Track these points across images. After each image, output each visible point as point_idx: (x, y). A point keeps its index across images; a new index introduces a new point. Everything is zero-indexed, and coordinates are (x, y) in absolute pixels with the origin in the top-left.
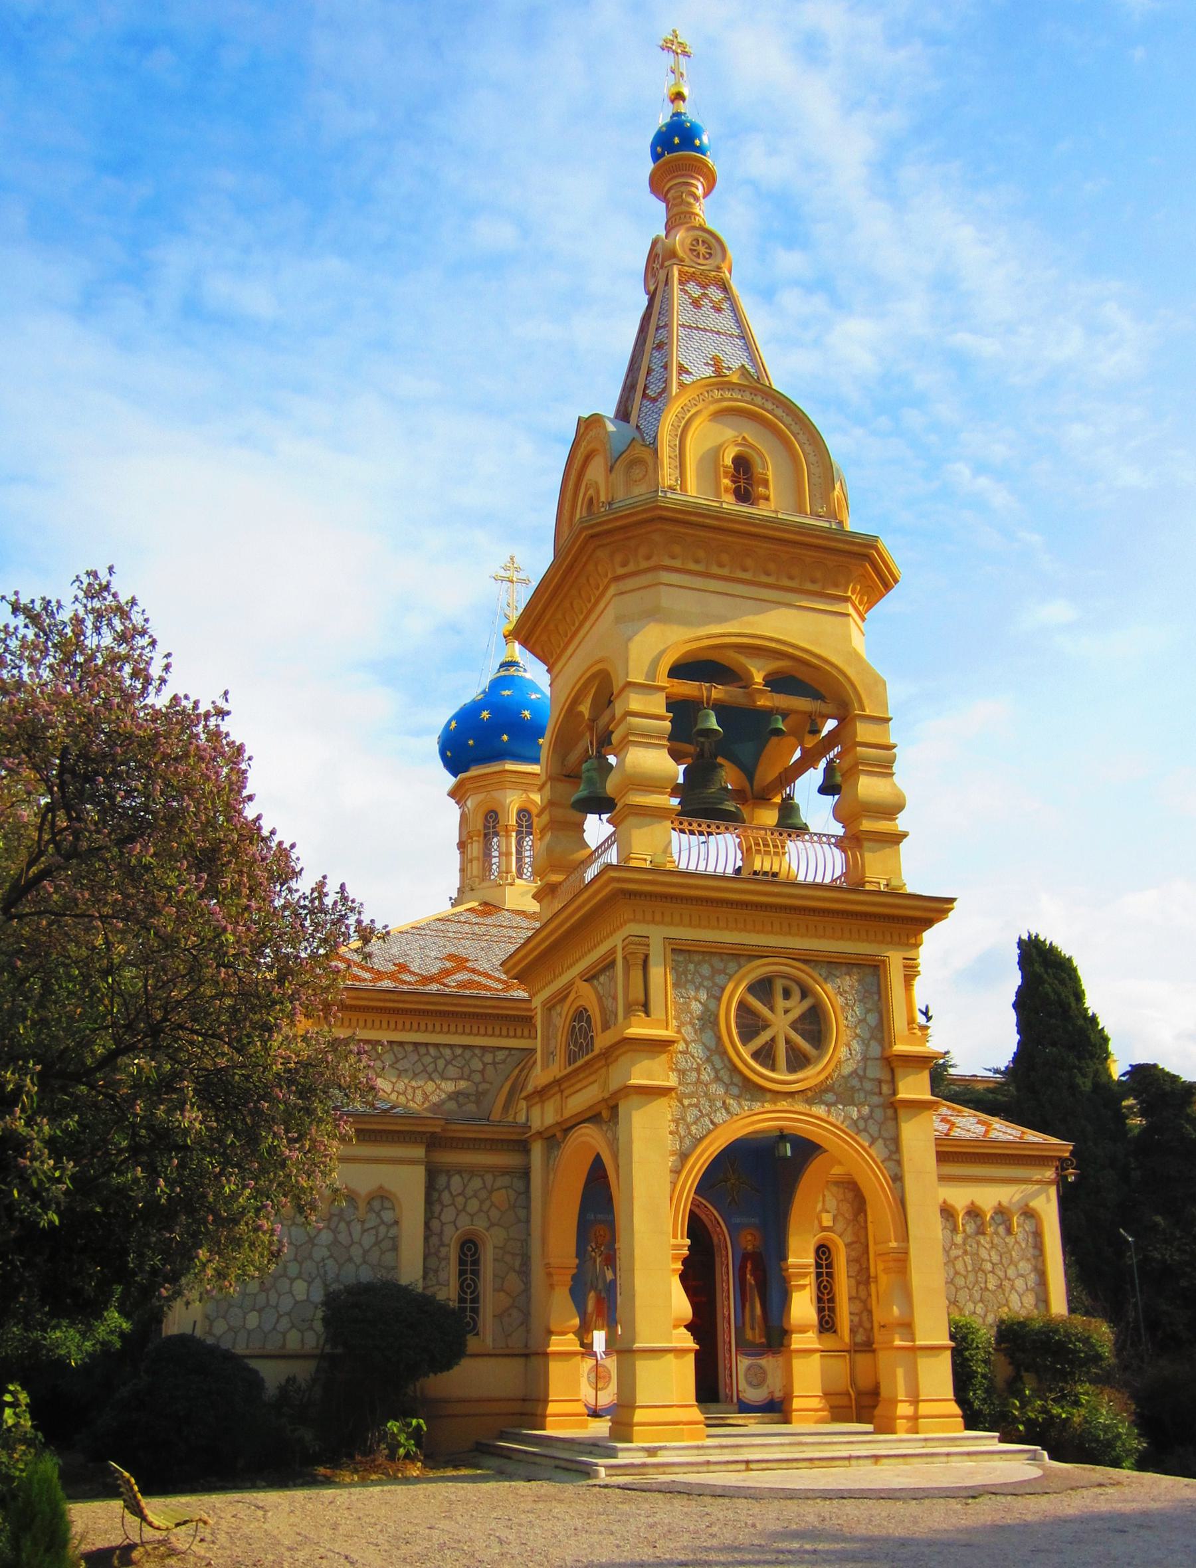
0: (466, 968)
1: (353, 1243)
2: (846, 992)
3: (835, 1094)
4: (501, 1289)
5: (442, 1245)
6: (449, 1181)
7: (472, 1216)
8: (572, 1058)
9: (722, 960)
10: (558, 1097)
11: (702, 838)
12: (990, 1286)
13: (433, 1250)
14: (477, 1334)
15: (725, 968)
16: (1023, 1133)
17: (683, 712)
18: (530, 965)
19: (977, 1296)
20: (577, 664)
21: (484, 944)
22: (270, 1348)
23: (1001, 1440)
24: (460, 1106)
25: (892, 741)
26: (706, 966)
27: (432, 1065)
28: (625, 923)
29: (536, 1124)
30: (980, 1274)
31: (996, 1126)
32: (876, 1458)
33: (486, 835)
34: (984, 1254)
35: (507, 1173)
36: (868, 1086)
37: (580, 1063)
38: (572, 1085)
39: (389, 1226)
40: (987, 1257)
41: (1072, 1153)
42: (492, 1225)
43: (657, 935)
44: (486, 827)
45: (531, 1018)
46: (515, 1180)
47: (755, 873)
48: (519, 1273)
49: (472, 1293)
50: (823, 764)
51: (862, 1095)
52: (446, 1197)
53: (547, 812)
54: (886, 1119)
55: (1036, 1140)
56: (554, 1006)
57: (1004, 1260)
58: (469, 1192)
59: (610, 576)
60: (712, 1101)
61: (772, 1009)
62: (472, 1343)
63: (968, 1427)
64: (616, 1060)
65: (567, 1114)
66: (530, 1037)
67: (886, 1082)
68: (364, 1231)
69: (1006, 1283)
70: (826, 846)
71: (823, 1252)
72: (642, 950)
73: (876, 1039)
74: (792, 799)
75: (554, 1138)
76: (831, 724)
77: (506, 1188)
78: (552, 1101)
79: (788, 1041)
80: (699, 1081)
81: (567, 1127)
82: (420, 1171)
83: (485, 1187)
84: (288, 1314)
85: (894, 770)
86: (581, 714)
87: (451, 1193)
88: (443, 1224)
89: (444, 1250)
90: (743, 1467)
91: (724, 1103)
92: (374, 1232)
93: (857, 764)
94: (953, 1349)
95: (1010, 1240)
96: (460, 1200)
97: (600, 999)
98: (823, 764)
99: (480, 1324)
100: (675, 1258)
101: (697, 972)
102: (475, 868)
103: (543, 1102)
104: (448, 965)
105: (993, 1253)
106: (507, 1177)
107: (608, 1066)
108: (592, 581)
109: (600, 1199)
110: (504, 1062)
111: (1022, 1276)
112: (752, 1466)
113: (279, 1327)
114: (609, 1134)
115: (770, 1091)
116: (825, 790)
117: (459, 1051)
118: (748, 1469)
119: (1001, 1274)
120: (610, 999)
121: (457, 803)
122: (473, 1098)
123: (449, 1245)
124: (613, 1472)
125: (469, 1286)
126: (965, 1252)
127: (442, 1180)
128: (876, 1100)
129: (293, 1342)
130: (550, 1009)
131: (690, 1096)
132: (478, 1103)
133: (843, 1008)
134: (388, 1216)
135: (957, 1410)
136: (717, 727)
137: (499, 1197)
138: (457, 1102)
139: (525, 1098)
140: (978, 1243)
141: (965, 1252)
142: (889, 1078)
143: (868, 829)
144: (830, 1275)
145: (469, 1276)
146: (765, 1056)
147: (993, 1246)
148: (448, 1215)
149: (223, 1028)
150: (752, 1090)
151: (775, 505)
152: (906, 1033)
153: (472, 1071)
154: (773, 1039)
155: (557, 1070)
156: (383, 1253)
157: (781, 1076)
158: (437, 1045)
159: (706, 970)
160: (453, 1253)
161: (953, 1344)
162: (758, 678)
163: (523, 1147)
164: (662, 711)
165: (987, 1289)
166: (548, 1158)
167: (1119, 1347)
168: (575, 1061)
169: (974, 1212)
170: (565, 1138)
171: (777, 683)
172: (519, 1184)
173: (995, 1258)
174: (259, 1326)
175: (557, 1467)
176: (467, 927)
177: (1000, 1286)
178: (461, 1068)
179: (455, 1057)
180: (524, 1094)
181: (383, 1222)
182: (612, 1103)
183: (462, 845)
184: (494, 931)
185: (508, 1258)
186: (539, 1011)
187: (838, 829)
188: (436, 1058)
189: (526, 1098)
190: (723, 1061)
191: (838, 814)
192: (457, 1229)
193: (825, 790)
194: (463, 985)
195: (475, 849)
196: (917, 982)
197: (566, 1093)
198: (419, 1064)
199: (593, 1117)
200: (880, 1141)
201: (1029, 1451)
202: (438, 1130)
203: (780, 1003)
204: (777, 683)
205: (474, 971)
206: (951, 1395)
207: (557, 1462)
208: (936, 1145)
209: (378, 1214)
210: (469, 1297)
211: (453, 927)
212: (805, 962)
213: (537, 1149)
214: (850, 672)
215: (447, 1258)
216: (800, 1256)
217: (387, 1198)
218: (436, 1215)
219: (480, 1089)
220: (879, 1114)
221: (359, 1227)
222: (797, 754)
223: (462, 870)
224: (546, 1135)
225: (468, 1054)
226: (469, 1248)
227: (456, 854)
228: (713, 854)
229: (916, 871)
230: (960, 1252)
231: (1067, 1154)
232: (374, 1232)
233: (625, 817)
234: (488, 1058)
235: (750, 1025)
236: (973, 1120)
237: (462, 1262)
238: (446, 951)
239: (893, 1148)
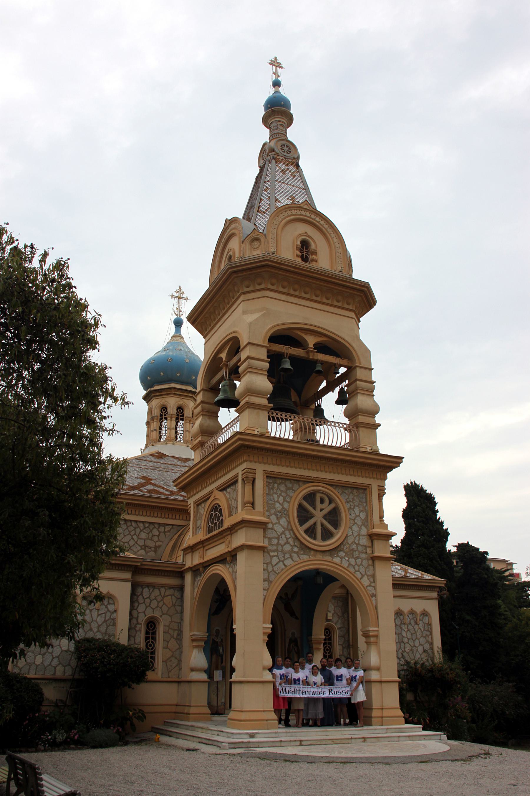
0: (151, 484)
1: (93, 621)
2: (350, 501)
3: (344, 552)
4: (167, 648)
5: (138, 623)
6: (142, 592)
7: (153, 609)
8: (210, 530)
9: (291, 483)
10: (202, 549)
11: (278, 423)
12: (407, 650)
13: (133, 626)
14: (154, 670)
15: (292, 487)
16: (422, 574)
17: (274, 359)
18: (191, 483)
20: (222, 332)
21: (159, 472)
22: (48, 675)
23: (424, 729)
24: (147, 553)
25: (373, 380)
26: (283, 485)
27: (134, 531)
28: (244, 462)
29: (189, 564)
30: (402, 644)
31: (409, 571)
32: (364, 739)
33: (161, 419)
34: (404, 634)
35: (172, 588)
36: (360, 548)
37: (215, 532)
38: (210, 544)
39: (112, 613)
40: (405, 636)
41: (446, 584)
42: (164, 614)
43: (260, 469)
44: (161, 415)
45: (187, 510)
46: (176, 591)
47: (307, 440)
48: (176, 639)
49: (152, 649)
50: (337, 390)
51: (357, 553)
52: (141, 600)
53: (200, 406)
54: (369, 565)
55: (428, 578)
56: (200, 504)
58: (152, 597)
59: (240, 292)
60: (285, 554)
61: (314, 508)
62: (150, 675)
63: (407, 722)
64: (237, 531)
65: (206, 559)
66: (186, 520)
67: (369, 547)
68: (99, 615)
69: (414, 648)
70: (342, 430)
71: (328, 631)
72: (252, 476)
73: (364, 525)
74: (321, 406)
75: (196, 571)
76: (342, 370)
77: (171, 595)
78: (198, 551)
79: (322, 525)
81: (206, 565)
82: (129, 585)
83: (161, 595)
84: (58, 657)
85: (374, 393)
86: (221, 358)
87: (143, 597)
88: (138, 613)
89: (138, 626)
91: (290, 555)
92: (103, 615)
93: (357, 390)
94: (399, 682)
95: (416, 627)
96: (148, 601)
97: (227, 500)
98: (337, 390)
99: (155, 666)
100: (264, 633)
101: (278, 488)
102: (155, 435)
103: (193, 552)
104: (143, 481)
106: (172, 590)
107: (231, 534)
108: (231, 294)
109: (220, 601)
110: (169, 531)
111: (421, 645)
113: (53, 664)
114: (231, 570)
115: (313, 550)
116: (338, 402)
117: (147, 525)
119: (412, 644)
120: (233, 501)
121: (147, 403)
122: (153, 549)
123: (141, 624)
124: (232, 746)
125: (150, 645)
127: (139, 590)
128: (363, 556)
129: (59, 673)
130: (198, 505)
131: (274, 551)
132: (155, 551)
133: (348, 509)
134: (111, 608)
135: (401, 713)
136: (290, 367)
137: (168, 600)
138: (145, 550)
139: (183, 550)
140: (401, 628)
142: (370, 545)
143: (362, 421)
144: (330, 644)
145: (151, 640)
147: (408, 630)
148: (141, 608)
149: (97, 503)
150: (305, 548)
151: (323, 262)
152: (379, 522)
153: (153, 536)
154: (315, 524)
155: (201, 536)
156: (108, 626)
157: (318, 543)
158: (136, 521)
159: (283, 487)
160: (143, 628)
161: (399, 680)
162: (311, 345)
163: (180, 574)
164: (265, 358)
165: (405, 651)
166: (194, 581)
168: (212, 532)
169: (412, 612)
170: (204, 571)
171: (320, 348)
172: (177, 594)
173: (409, 636)
174: (42, 663)
175: (199, 742)
176: (151, 464)
177: (411, 650)
178: (148, 534)
179: (145, 528)
180: (182, 548)
181: (109, 611)
182: (233, 553)
183: (148, 423)
184: (163, 466)
185: (171, 632)
186: (192, 505)
187: (346, 421)
188: (135, 528)
189: (184, 550)
190: (290, 534)
191: (347, 414)
192: (146, 616)
193: (338, 402)
194: (150, 491)
195: (155, 425)
196: (385, 498)
197: (206, 548)
198: (127, 530)
199: (221, 560)
200: (366, 576)
201: (437, 735)
202: (139, 564)
203: (319, 506)
204: (320, 348)
205: (155, 485)
206: (398, 706)
207: (200, 740)
208: (393, 580)
209: (106, 607)
210: (150, 651)
211: (144, 463)
212: (331, 485)
213: (188, 577)
214: (354, 345)
215: (140, 630)
216: (318, 633)
217: (111, 598)
218: (135, 608)
219: (157, 545)
220: (365, 563)
221: (96, 613)
222: (324, 384)
223: (147, 436)
224: (194, 569)
225: (151, 527)
226: (151, 625)
227: (145, 427)
228: (283, 430)
229: (386, 444)
231: (443, 585)
232: (103, 615)
233: (246, 408)
234: (162, 529)
235: (304, 515)
236: (399, 568)
237: (147, 633)
238: (142, 475)
239: (372, 580)
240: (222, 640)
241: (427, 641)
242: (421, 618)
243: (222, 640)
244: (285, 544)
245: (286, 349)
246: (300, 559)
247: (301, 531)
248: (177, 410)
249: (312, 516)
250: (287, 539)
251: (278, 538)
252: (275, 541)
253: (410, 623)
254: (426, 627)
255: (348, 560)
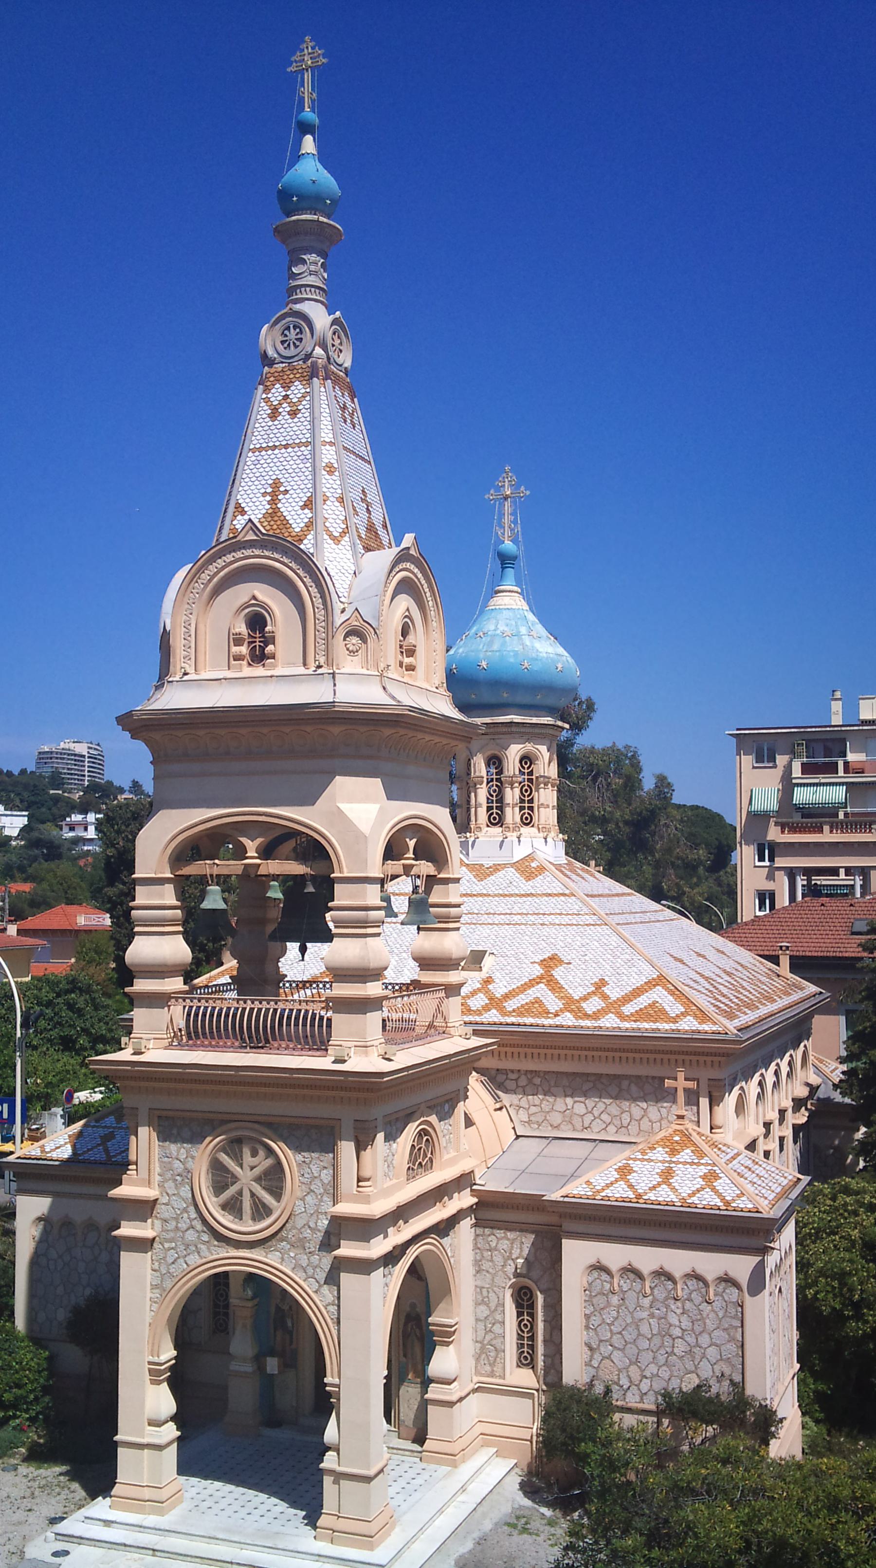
19: (662, 1359)
30: (667, 1338)
57: (696, 1327)
61: (241, 1166)
79: (253, 1195)
80: (177, 1228)
90: (151, 1552)
105: (684, 1318)
112: (156, 1553)
118: (153, 1555)
126: (652, 1316)
141: (652, 1316)
146: (232, 1207)
154: (240, 1193)
157: (247, 1226)
167: (576, 1511)
173: (686, 1323)
230: (645, 1315)
240: (290, 1307)
241: (732, 1339)
242: (720, 1289)
243: (290, 1307)
244: (188, 1229)
245: (211, 868)
246: (201, 1257)
247: (212, 1204)
248: (521, 762)
249: (235, 1179)
250: (191, 1220)
251: (176, 1219)
252: (172, 1225)
253: (690, 1299)
254: (732, 1311)
255: (294, 1258)
